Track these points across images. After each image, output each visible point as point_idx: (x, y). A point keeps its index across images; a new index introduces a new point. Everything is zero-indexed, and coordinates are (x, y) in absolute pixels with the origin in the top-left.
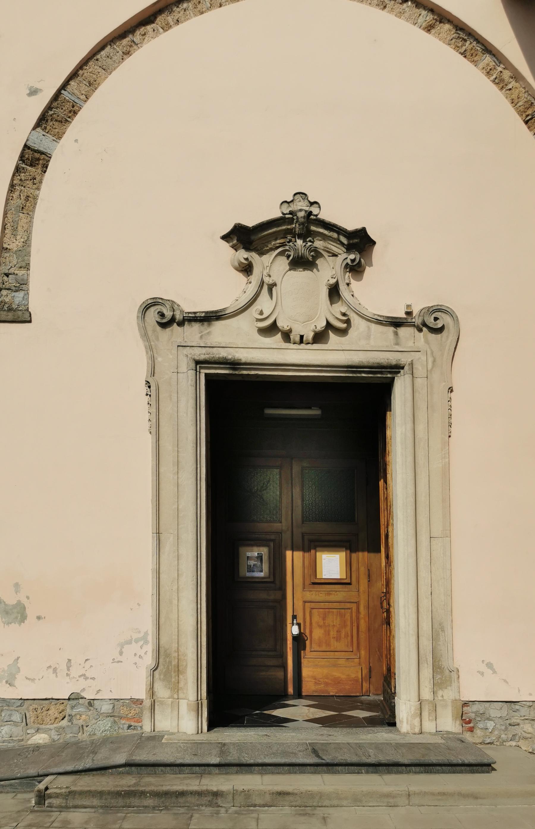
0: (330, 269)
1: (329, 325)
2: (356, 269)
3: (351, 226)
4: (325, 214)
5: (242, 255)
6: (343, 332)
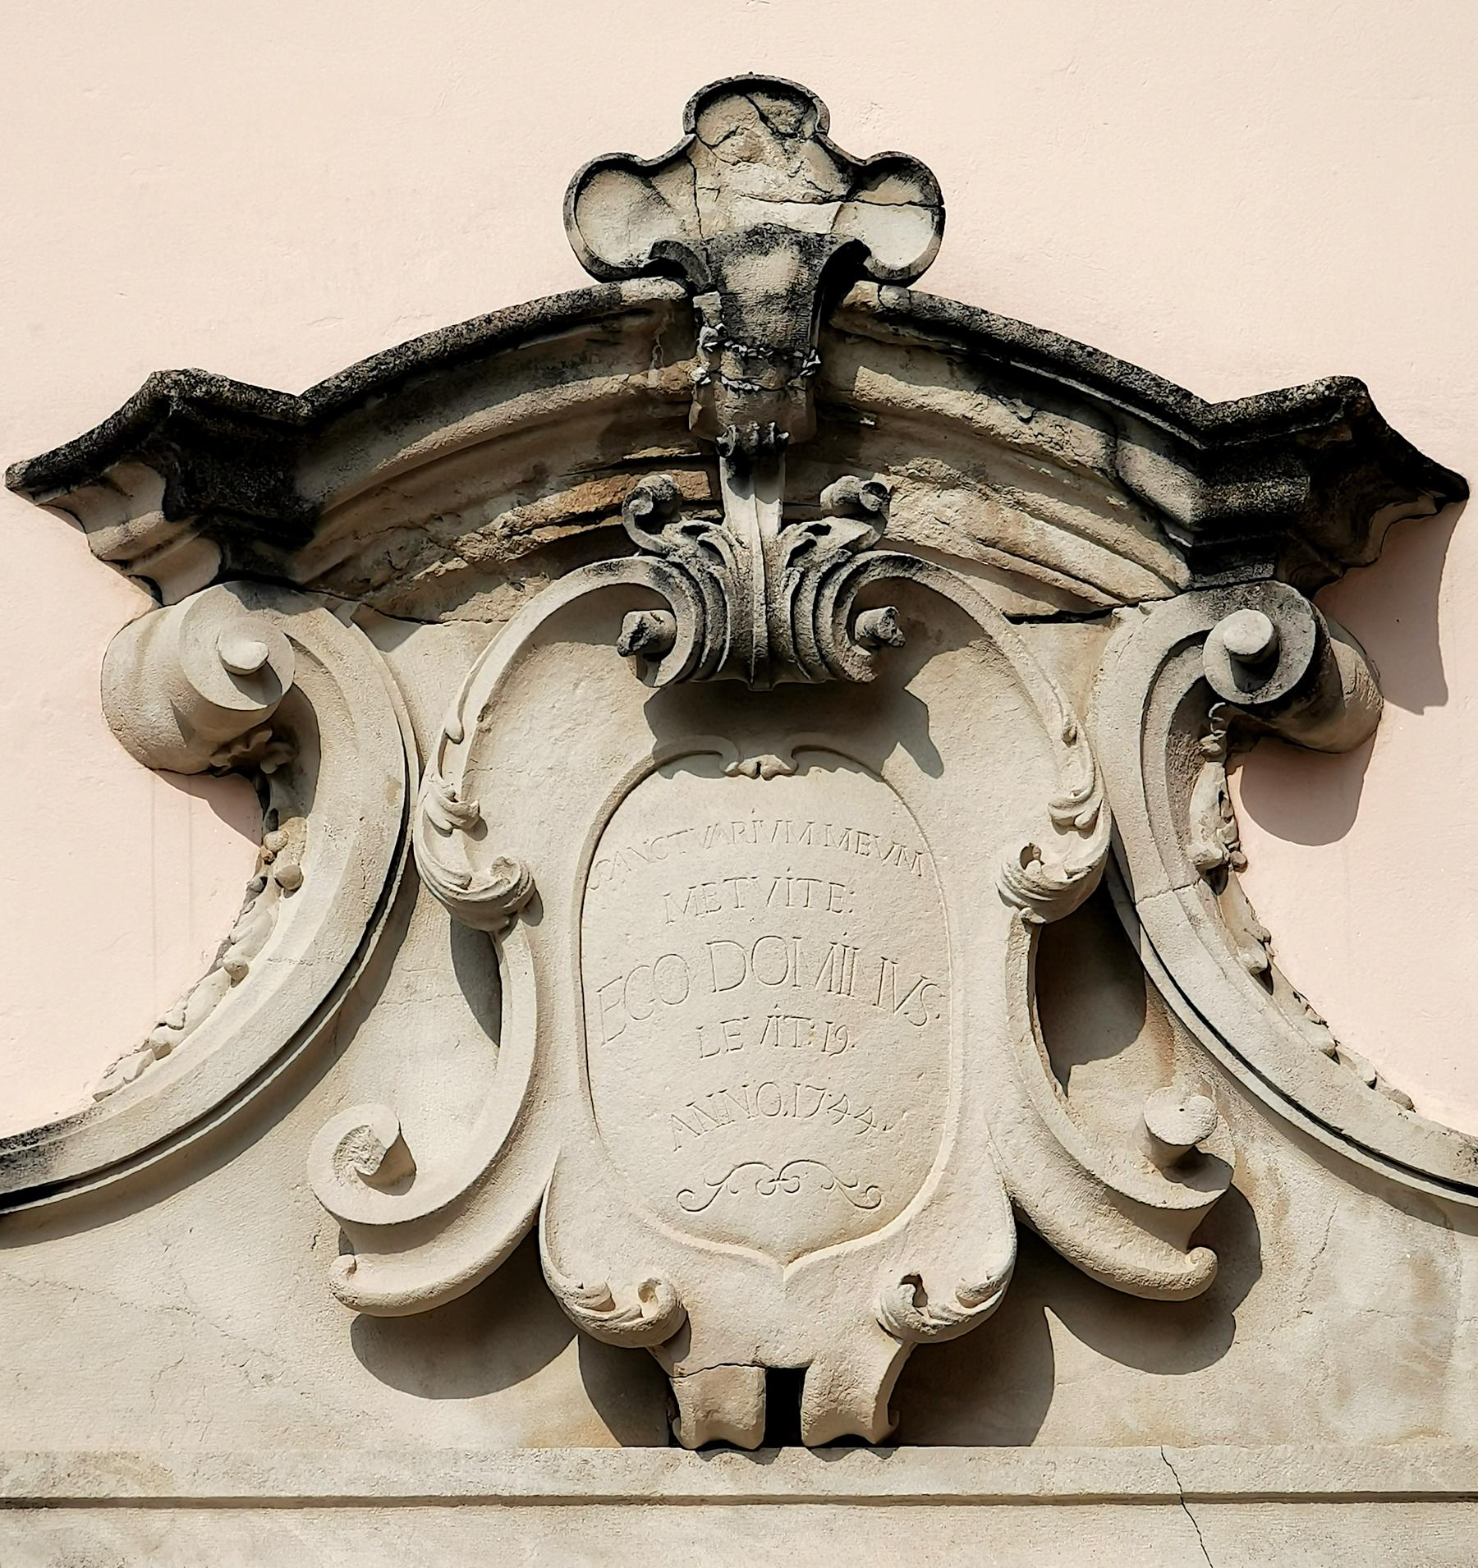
0: (1042, 739)
1: (1039, 1262)
2: (1285, 737)
3: (1226, 365)
4: (983, 270)
5: (217, 638)
6: (1179, 1326)
